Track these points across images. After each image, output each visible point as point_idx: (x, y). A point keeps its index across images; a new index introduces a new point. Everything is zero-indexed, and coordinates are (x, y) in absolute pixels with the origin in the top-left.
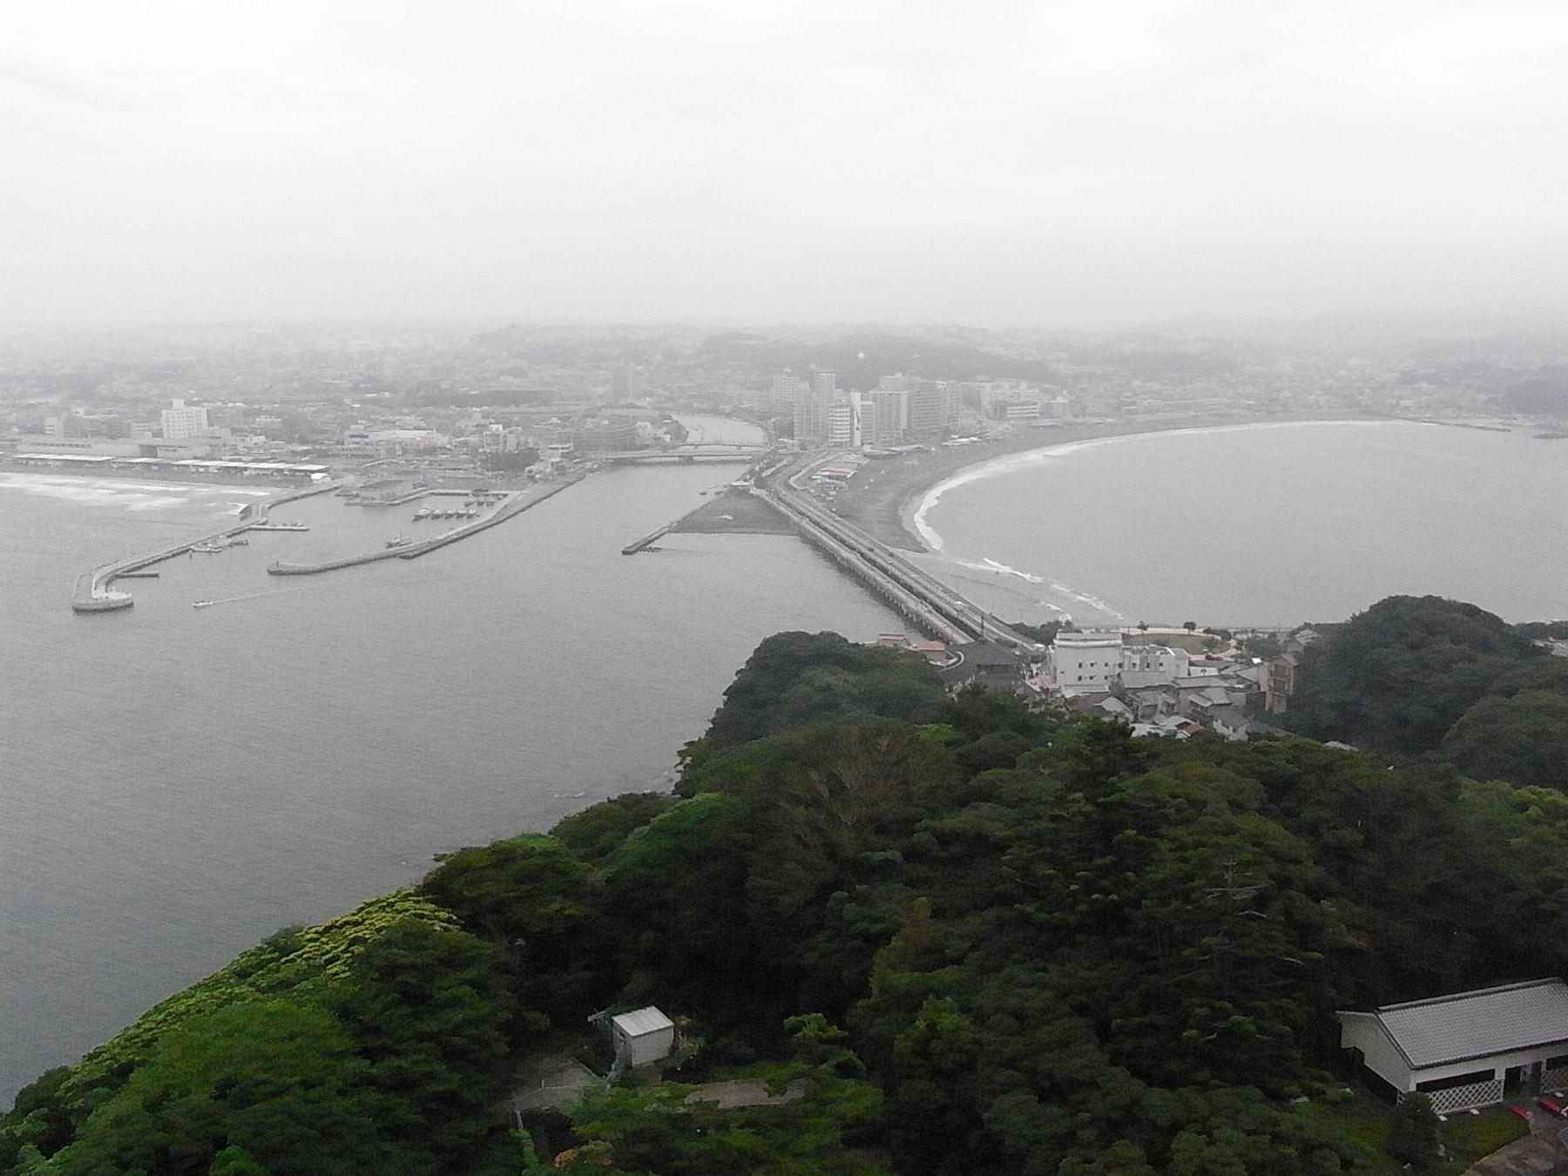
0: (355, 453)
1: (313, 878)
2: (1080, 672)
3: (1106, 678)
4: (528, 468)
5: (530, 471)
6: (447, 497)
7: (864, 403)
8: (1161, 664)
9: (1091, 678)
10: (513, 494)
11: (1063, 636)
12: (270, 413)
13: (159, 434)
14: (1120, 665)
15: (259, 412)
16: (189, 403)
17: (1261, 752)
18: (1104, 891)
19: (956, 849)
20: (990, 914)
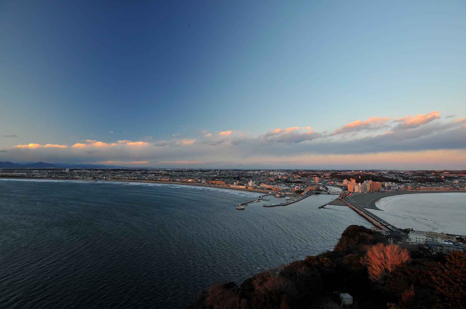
2: (417, 240)
9: (419, 241)
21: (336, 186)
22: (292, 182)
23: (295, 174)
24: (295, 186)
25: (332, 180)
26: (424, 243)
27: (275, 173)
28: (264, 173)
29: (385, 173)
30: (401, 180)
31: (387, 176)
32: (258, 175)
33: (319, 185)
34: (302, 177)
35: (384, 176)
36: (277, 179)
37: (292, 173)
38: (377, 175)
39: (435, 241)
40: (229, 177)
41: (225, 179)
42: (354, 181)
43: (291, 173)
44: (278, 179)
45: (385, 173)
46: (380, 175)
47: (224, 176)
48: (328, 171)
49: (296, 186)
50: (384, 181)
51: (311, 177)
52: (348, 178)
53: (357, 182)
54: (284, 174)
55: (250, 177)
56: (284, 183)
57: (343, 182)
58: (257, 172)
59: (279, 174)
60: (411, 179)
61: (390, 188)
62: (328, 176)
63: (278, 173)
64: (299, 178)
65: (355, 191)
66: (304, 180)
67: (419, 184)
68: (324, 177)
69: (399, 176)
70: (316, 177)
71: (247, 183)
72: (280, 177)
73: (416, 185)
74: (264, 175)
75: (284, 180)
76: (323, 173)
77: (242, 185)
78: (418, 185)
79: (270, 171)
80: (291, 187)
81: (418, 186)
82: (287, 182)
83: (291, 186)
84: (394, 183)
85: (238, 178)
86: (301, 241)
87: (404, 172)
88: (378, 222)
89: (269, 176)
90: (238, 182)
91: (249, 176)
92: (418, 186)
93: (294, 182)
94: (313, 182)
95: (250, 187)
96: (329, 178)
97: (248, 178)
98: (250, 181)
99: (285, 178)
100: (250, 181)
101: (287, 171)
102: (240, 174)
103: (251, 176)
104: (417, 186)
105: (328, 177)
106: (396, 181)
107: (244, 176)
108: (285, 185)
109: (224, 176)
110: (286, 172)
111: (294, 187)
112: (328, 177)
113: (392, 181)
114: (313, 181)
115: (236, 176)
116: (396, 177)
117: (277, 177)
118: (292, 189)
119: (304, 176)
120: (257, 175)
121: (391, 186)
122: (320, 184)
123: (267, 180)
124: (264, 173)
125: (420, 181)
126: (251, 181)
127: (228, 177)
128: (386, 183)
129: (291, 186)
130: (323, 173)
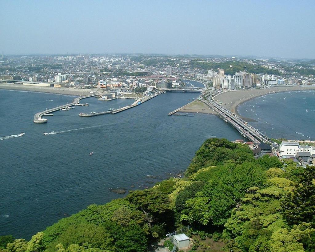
0: (101, 87)
1: (64, 230)
2: (288, 152)
3: (294, 153)
4: (144, 92)
5: (145, 93)
6: (183, 241)
7: (232, 78)
8: (309, 151)
9: (290, 153)
10: (140, 99)
11: (284, 142)
12: (80, 76)
13: (54, 81)
14: (298, 150)
15: (78, 76)
16: (62, 74)
17: (85, 125)
18: (307, 210)
19: (266, 198)
20: (275, 215)
21: (197, 79)
22: (128, 75)
23: (135, 60)
24: (134, 80)
25: (192, 70)
26: (295, 155)
27: (102, 58)
28: (83, 60)
29: (265, 61)
30: (282, 71)
31: (266, 66)
32: (72, 63)
33: (171, 79)
34: (145, 65)
35: (263, 65)
36: (105, 69)
37: (130, 59)
38: (253, 64)
39: (306, 151)
40: (22, 68)
41: (14, 70)
42: (222, 72)
43: (129, 59)
44: (106, 69)
45: (264, 61)
46: (257, 64)
47: (12, 66)
48: (186, 57)
49: (136, 81)
50: (261, 73)
51: (160, 65)
52: (216, 67)
53: (227, 74)
54: (117, 60)
55: (57, 68)
56: (116, 76)
57: (207, 73)
58: (70, 57)
59: (109, 61)
60: (294, 71)
61: (268, 82)
62: (186, 64)
63: (108, 58)
64: (141, 68)
65: (111, 82)
66: (150, 71)
67: (302, 77)
68: (181, 65)
69: (281, 65)
70: (168, 65)
71: (53, 77)
72: (109, 67)
73: (298, 79)
74: (84, 63)
75: (117, 71)
76: (180, 60)
77: (44, 82)
78: (300, 79)
79: (93, 56)
80: (126, 82)
81: (300, 79)
82: (121, 74)
83: (128, 80)
84: (273, 76)
85: (38, 70)
86: (98, 124)
87: (287, 60)
88: (247, 131)
89: (92, 63)
90: (36, 75)
91: (57, 65)
92: (300, 79)
93: (132, 74)
94: (163, 74)
95: (57, 84)
96: (188, 68)
97: (54, 68)
98: (57, 74)
99: (118, 67)
100: (57, 74)
101: (122, 56)
102: (40, 62)
103: (61, 65)
104: (299, 79)
105: (186, 65)
106: (276, 73)
107: (47, 66)
108: (116, 80)
109: (12, 66)
110: (121, 57)
111: (132, 81)
112: (186, 65)
113: (270, 72)
114: (163, 73)
115: (34, 66)
116: (277, 67)
117: (105, 65)
118: (129, 85)
119: (152, 63)
120: (71, 62)
121: (269, 81)
122: (174, 77)
123: (87, 71)
124: (82, 59)
125: (302, 72)
126: (59, 74)
127: (19, 68)
128: (264, 75)
129: (128, 80)
130: (180, 60)
